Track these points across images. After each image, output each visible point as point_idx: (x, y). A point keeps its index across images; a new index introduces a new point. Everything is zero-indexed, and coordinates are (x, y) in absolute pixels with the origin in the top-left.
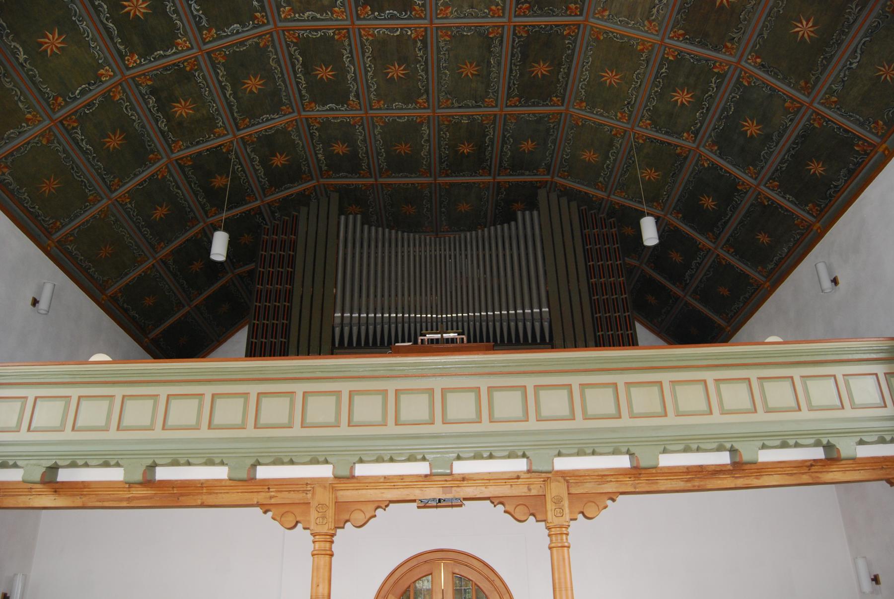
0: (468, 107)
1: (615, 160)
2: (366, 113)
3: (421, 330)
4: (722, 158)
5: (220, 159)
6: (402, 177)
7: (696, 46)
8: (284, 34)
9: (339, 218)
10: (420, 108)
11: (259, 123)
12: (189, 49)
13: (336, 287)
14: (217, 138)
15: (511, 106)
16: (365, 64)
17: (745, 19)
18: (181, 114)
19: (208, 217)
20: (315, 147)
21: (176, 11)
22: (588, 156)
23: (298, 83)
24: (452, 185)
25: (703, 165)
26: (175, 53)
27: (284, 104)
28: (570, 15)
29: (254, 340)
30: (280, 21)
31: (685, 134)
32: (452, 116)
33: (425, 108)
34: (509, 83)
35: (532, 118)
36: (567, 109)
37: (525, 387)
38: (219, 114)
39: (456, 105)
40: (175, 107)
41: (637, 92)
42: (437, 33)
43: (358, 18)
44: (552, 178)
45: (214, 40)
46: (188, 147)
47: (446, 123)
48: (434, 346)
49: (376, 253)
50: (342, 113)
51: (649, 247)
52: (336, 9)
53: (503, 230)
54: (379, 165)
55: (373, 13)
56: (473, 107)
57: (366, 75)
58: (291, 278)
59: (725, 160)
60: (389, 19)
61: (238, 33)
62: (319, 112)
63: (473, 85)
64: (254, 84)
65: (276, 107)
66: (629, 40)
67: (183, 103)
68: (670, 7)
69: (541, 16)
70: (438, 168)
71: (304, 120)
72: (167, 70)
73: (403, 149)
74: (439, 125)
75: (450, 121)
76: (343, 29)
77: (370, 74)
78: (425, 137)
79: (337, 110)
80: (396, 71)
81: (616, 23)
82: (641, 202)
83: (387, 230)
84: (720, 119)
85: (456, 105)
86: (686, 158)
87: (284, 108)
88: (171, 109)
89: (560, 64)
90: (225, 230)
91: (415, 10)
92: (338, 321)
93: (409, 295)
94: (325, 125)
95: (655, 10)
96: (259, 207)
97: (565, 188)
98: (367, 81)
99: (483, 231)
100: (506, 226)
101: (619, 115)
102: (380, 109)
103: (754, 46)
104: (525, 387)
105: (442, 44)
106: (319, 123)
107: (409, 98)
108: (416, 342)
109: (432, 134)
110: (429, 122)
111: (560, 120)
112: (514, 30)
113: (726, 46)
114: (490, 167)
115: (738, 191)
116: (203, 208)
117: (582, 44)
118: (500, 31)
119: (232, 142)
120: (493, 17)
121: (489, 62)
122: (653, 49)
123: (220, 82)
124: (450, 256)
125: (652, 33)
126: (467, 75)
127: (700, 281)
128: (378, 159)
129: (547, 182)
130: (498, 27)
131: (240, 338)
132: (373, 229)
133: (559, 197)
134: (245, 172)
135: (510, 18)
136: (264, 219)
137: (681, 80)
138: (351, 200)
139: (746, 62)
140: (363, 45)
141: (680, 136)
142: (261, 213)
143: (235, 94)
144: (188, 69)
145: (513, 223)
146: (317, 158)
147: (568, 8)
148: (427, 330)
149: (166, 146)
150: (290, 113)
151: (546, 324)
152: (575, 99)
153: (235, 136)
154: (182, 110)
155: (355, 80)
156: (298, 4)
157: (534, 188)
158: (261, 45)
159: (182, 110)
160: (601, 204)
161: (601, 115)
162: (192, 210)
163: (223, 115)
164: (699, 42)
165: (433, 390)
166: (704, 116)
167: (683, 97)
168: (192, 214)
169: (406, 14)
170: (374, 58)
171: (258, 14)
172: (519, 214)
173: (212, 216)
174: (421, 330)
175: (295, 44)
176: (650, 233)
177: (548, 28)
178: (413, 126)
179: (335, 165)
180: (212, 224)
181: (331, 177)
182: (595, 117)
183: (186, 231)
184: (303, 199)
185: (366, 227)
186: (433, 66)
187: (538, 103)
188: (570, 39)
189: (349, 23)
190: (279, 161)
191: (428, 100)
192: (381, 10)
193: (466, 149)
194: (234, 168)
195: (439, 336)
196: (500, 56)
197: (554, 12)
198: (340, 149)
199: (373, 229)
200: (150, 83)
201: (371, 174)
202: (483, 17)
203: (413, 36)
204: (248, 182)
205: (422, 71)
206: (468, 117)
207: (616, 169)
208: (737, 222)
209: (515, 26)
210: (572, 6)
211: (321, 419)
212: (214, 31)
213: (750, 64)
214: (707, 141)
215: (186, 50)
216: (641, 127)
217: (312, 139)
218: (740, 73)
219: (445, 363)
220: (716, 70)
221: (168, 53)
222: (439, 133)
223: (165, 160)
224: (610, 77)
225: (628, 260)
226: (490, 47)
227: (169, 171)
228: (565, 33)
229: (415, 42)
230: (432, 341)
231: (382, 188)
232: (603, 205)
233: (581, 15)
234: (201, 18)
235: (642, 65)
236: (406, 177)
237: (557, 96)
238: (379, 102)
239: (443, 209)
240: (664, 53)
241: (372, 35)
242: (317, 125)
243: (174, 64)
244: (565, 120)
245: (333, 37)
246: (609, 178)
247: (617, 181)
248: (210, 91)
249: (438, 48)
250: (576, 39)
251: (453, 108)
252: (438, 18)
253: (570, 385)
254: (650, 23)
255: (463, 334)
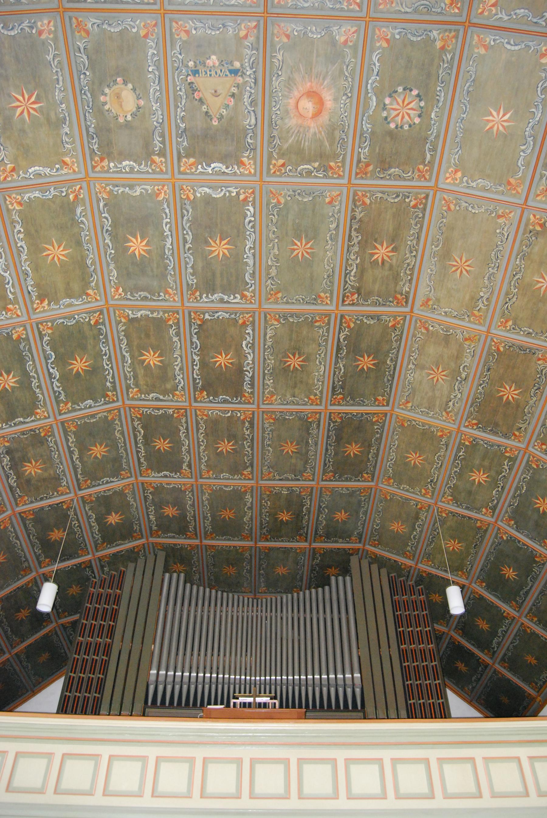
0: (287, 479)
1: (421, 532)
2: (197, 481)
3: (234, 692)
4: (519, 532)
5: (60, 514)
6: (225, 540)
7: (489, 434)
8: (130, 411)
9: (163, 575)
10: (245, 479)
11: (99, 485)
12: (46, 418)
13: (154, 643)
14: (60, 495)
15: (326, 480)
16: (198, 439)
17: (529, 413)
18: (30, 473)
19: (41, 568)
20: (147, 509)
21: (39, 387)
22: (396, 527)
23: (138, 452)
24: (270, 549)
25: (502, 537)
26: (33, 421)
27: (123, 470)
28: (378, 406)
29: (68, 694)
30: (128, 399)
31: (484, 510)
32: (274, 487)
33: (249, 479)
34: (325, 460)
35: (345, 492)
36: (377, 484)
37: (335, 760)
38: (65, 475)
39: (277, 477)
40: (26, 466)
41: (439, 471)
42: (263, 416)
43: (196, 401)
44: (364, 545)
45: (69, 412)
46: (32, 502)
47: (268, 493)
48: (247, 710)
49: (196, 611)
50: (174, 480)
51: (456, 616)
52: (177, 392)
53: (317, 593)
54: (205, 528)
55: (208, 397)
56: (292, 480)
57: (199, 447)
58: (111, 632)
59: (522, 534)
60: (222, 403)
61: (90, 407)
62: (155, 478)
63: (293, 461)
64: (99, 451)
65: (116, 473)
66: (430, 427)
67: (34, 463)
68: (464, 402)
69: (352, 405)
70: (258, 534)
71: (140, 484)
72: (24, 434)
73: (228, 514)
74: (261, 495)
75: (271, 492)
76: (182, 409)
77: (202, 448)
78: (249, 504)
79: (170, 477)
80: (226, 446)
81: (418, 413)
82: (446, 571)
83: (208, 590)
84: (514, 497)
85: (277, 477)
86: (486, 531)
87: (123, 472)
88: (22, 467)
89: (370, 446)
90: (55, 582)
91: (244, 396)
92: (153, 678)
93: (225, 655)
94: (158, 490)
95: (451, 404)
96: (90, 561)
97: (376, 556)
98: (199, 453)
99: (298, 594)
100: (320, 590)
101: (423, 491)
102: (209, 478)
103: (539, 435)
104: (335, 760)
105: (267, 425)
106: (153, 487)
107: (235, 469)
108: (228, 706)
109: (254, 502)
110: (252, 490)
111: (371, 493)
112: (330, 416)
113: (514, 434)
114: (307, 534)
115: (536, 562)
116: (38, 559)
117: (389, 429)
118: (317, 416)
119: (72, 500)
120: (311, 405)
121: (307, 442)
122: (451, 435)
123: (69, 448)
124: (266, 617)
125: (449, 422)
126: (288, 451)
127: (508, 649)
128: (204, 523)
129: (359, 549)
130: (316, 413)
131: (53, 692)
132: (195, 587)
133: (370, 564)
134: (81, 528)
135: (326, 406)
136: (93, 572)
137: (477, 462)
138: (175, 558)
139: (533, 448)
140: (198, 423)
141: (479, 510)
142: (91, 567)
143: (81, 458)
144: (42, 434)
145: (327, 588)
146: (149, 518)
147: (376, 400)
148: (240, 692)
149: (12, 499)
150: (128, 477)
151: (358, 691)
152: (384, 476)
153: (76, 495)
154: (32, 469)
155: (189, 452)
156: (145, 387)
157: (347, 554)
158: (109, 418)
159: (32, 469)
160: (409, 572)
161: (407, 491)
162: (27, 560)
163: (68, 477)
164: (491, 430)
165: (241, 759)
166: (500, 494)
167: (479, 477)
168: (26, 564)
169: (237, 399)
170: (207, 435)
171: (110, 393)
172: (333, 579)
173: (45, 567)
174: (234, 692)
175: (139, 419)
176: (456, 604)
177: (360, 415)
178: (238, 495)
179: (164, 526)
180: (43, 574)
181: (159, 537)
182: (401, 492)
183: (18, 580)
184: (131, 556)
185: (188, 585)
186: (258, 443)
187: (351, 479)
188: (378, 425)
189: (187, 404)
190: (113, 519)
191: (252, 473)
192: (216, 395)
193: (285, 517)
194: (71, 523)
195: (250, 700)
196: (318, 437)
197: (364, 402)
198: (170, 511)
199: (195, 587)
200: (7, 444)
201: (196, 534)
202: (303, 405)
203: (242, 418)
204: (83, 536)
205: (249, 447)
206: (288, 489)
207: (422, 540)
208: (536, 594)
209: (330, 413)
210: (380, 398)
211: (124, 787)
212: (70, 404)
213: (537, 450)
214: (504, 516)
215: (43, 419)
216: (444, 502)
217: (146, 501)
218: (529, 457)
219: (255, 731)
220: (507, 455)
221: (27, 420)
222: (261, 502)
223: (9, 512)
224: (414, 458)
225: (437, 627)
226: (308, 429)
227: (12, 523)
228: (374, 420)
229: (243, 422)
230: (244, 705)
231: (206, 549)
232: (412, 572)
233: (388, 405)
234: (60, 393)
235: (442, 448)
236: (229, 540)
237: (367, 473)
238: (208, 472)
239: (262, 572)
240: (461, 439)
241: (206, 416)
242: (152, 490)
243: (31, 430)
244: (375, 494)
245: (172, 415)
246: (416, 548)
247: (423, 550)
248: (59, 454)
249: (263, 428)
250: (384, 425)
251: (274, 480)
252: (264, 404)
253: (382, 759)
254: (448, 413)
255: (275, 698)
